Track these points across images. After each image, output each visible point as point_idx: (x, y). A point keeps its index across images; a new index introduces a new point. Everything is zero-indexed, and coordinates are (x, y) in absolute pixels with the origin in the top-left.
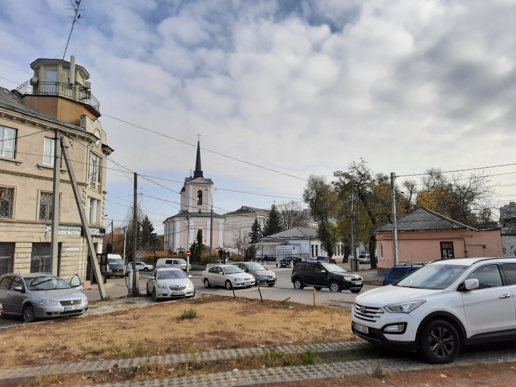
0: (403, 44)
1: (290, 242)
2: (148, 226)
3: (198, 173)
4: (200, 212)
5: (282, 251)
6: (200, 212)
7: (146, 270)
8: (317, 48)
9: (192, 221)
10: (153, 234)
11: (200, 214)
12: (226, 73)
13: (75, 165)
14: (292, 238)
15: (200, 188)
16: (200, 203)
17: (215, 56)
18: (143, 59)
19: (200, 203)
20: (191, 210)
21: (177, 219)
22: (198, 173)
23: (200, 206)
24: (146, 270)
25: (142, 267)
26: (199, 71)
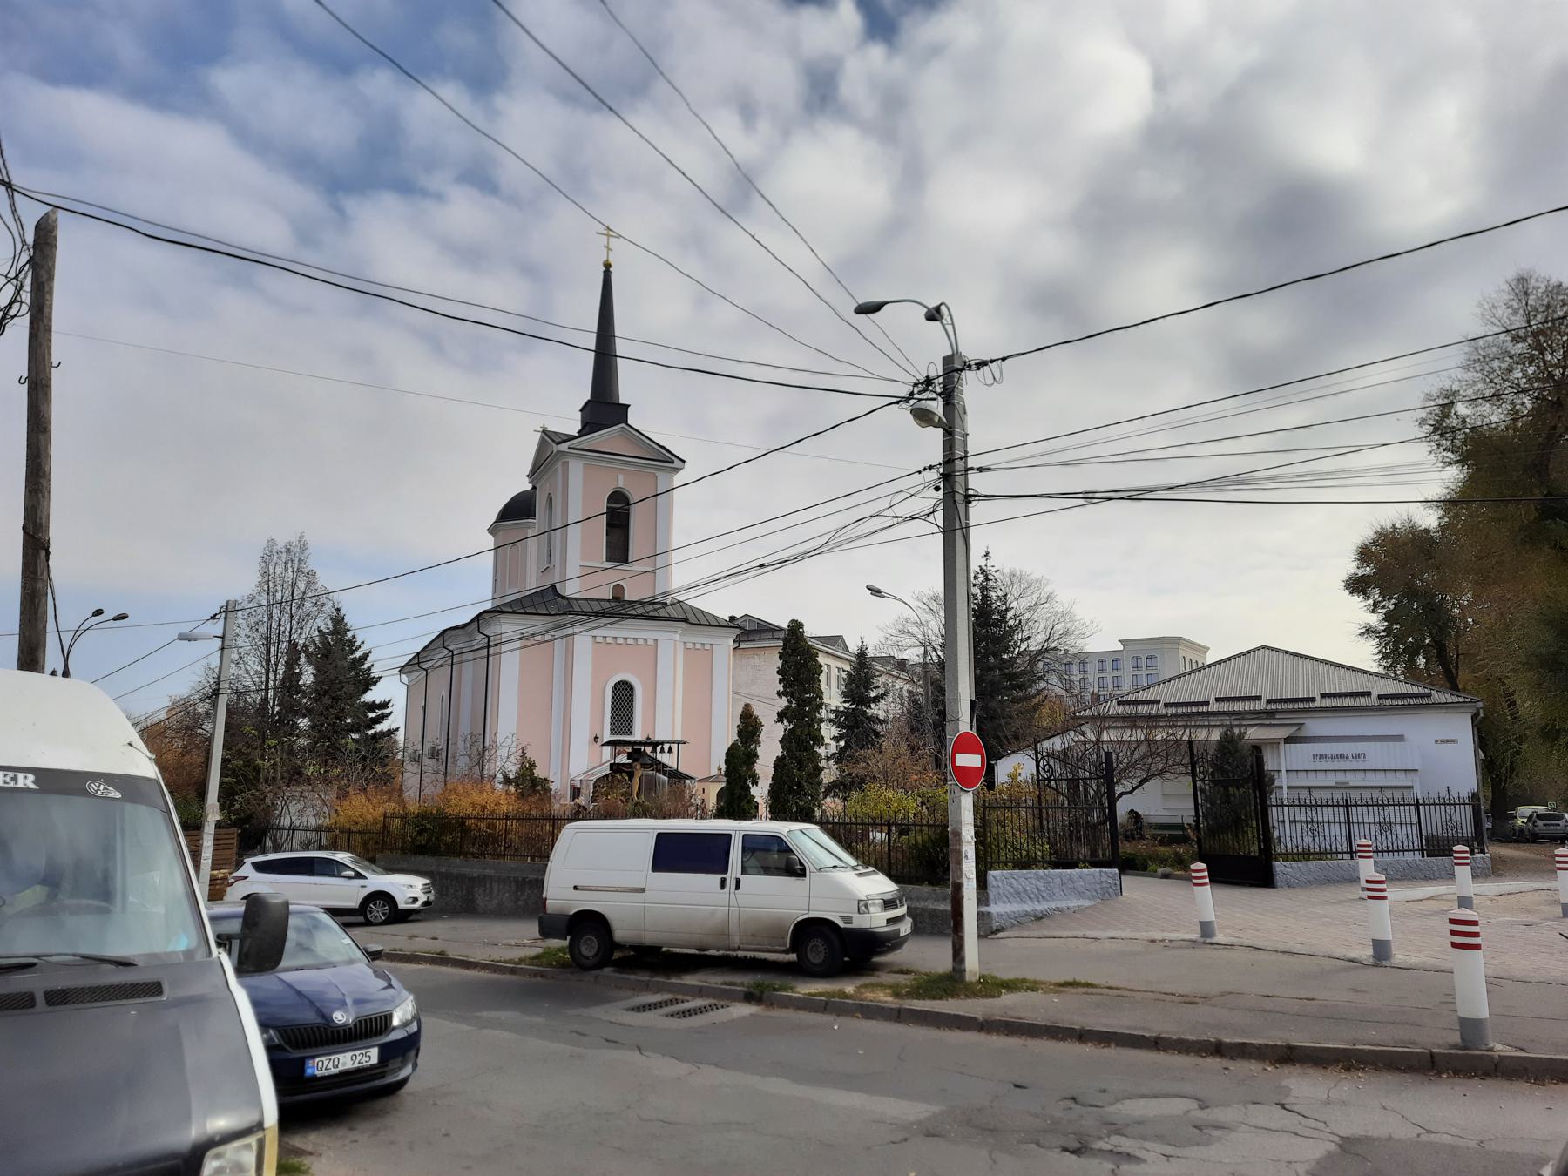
0: (1114, 93)
1: (1315, 726)
2: (340, 666)
3: (604, 409)
4: (618, 598)
5: (1330, 780)
6: (618, 598)
7: (378, 911)
8: (821, 91)
9: (585, 642)
10: (373, 706)
11: (618, 609)
12: (479, 178)
13: (248, 1146)
14: (1320, 703)
15: (622, 482)
16: (618, 550)
17: (431, 112)
18: (150, 94)
19: (618, 550)
20: (571, 589)
21: (508, 627)
22: (604, 409)
23: (617, 574)
24: (378, 911)
25: (348, 892)
26: (375, 168)
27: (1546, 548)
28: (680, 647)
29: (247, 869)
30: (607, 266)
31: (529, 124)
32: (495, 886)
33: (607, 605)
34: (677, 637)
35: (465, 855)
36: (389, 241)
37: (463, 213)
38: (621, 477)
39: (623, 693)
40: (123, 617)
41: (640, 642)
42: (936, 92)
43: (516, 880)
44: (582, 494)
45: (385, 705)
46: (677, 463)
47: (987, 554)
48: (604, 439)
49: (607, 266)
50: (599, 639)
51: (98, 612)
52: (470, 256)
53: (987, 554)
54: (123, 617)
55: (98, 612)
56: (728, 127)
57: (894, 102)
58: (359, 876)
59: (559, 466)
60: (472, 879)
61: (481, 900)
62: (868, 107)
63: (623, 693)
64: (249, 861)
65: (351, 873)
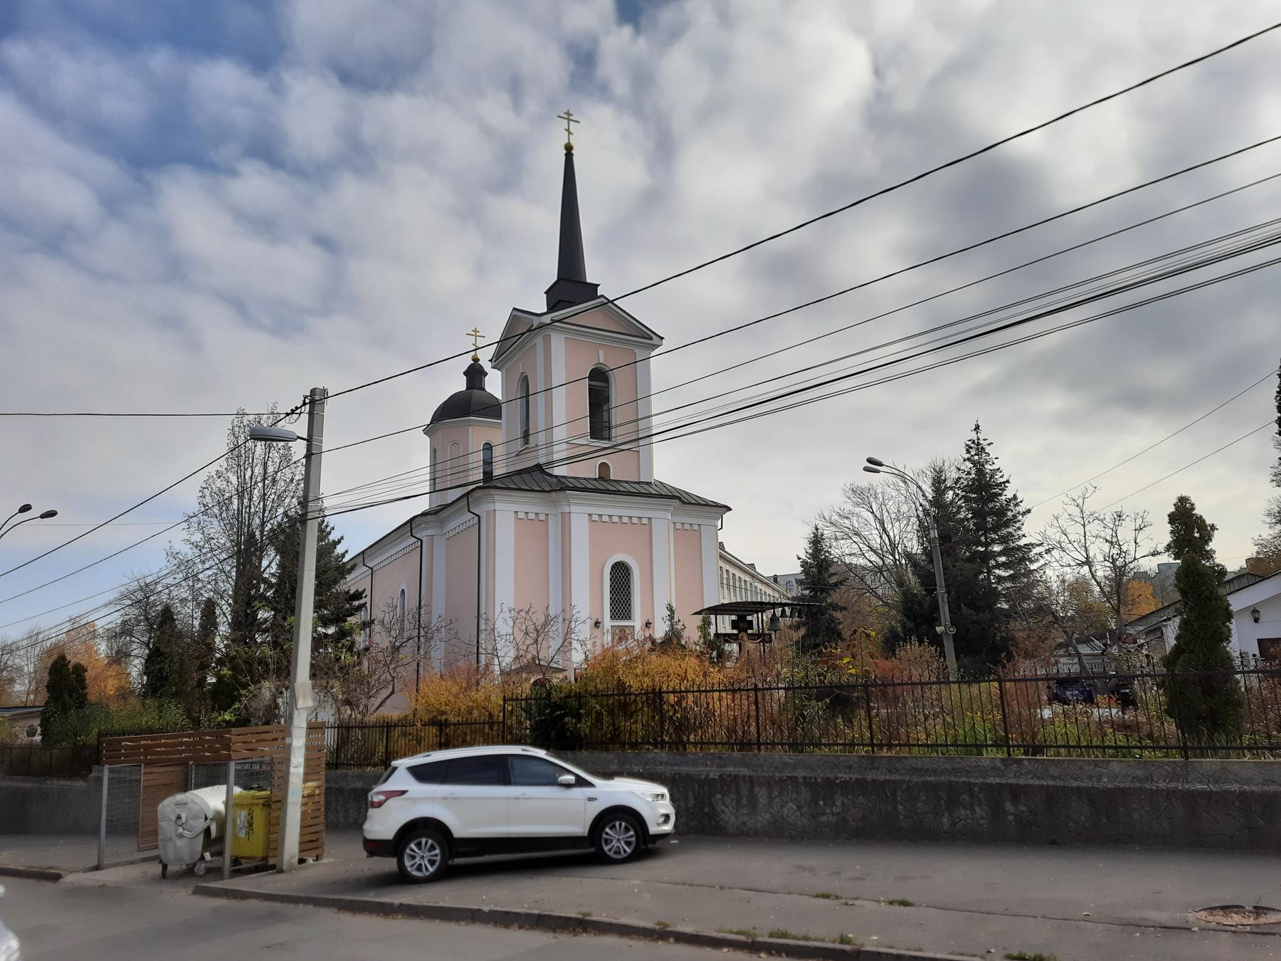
3: (571, 287)
11: (603, 486)
15: (602, 358)
19: (599, 426)
22: (571, 287)
27: (101, 631)
28: (672, 526)
29: (401, 778)
30: (569, 148)
31: (312, 112)
32: (762, 794)
33: (595, 483)
34: (669, 516)
35: (1215, 749)
36: (192, 213)
37: (256, 186)
38: (601, 353)
39: (621, 574)
40: (51, 514)
41: (635, 521)
42: (680, 70)
43: (810, 783)
44: (563, 364)
45: (358, 595)
46: (656, 340)
47: (977, 428)
48: (582, 313)
49: (569, 148)
50: (595, 518)
51: (25, 508)
52: (264, 226)
53: (977, 428)
54: (51, 514)
55: (25, 508)
56: (496, 110)
57: (643, 79)
58: (581, 782)
59: (539, 341)
60: (708, 782)
61: (729, 813)
62: (621, 86)
63: (621, 574)
64: (403, 764)
65: (571, 778)
